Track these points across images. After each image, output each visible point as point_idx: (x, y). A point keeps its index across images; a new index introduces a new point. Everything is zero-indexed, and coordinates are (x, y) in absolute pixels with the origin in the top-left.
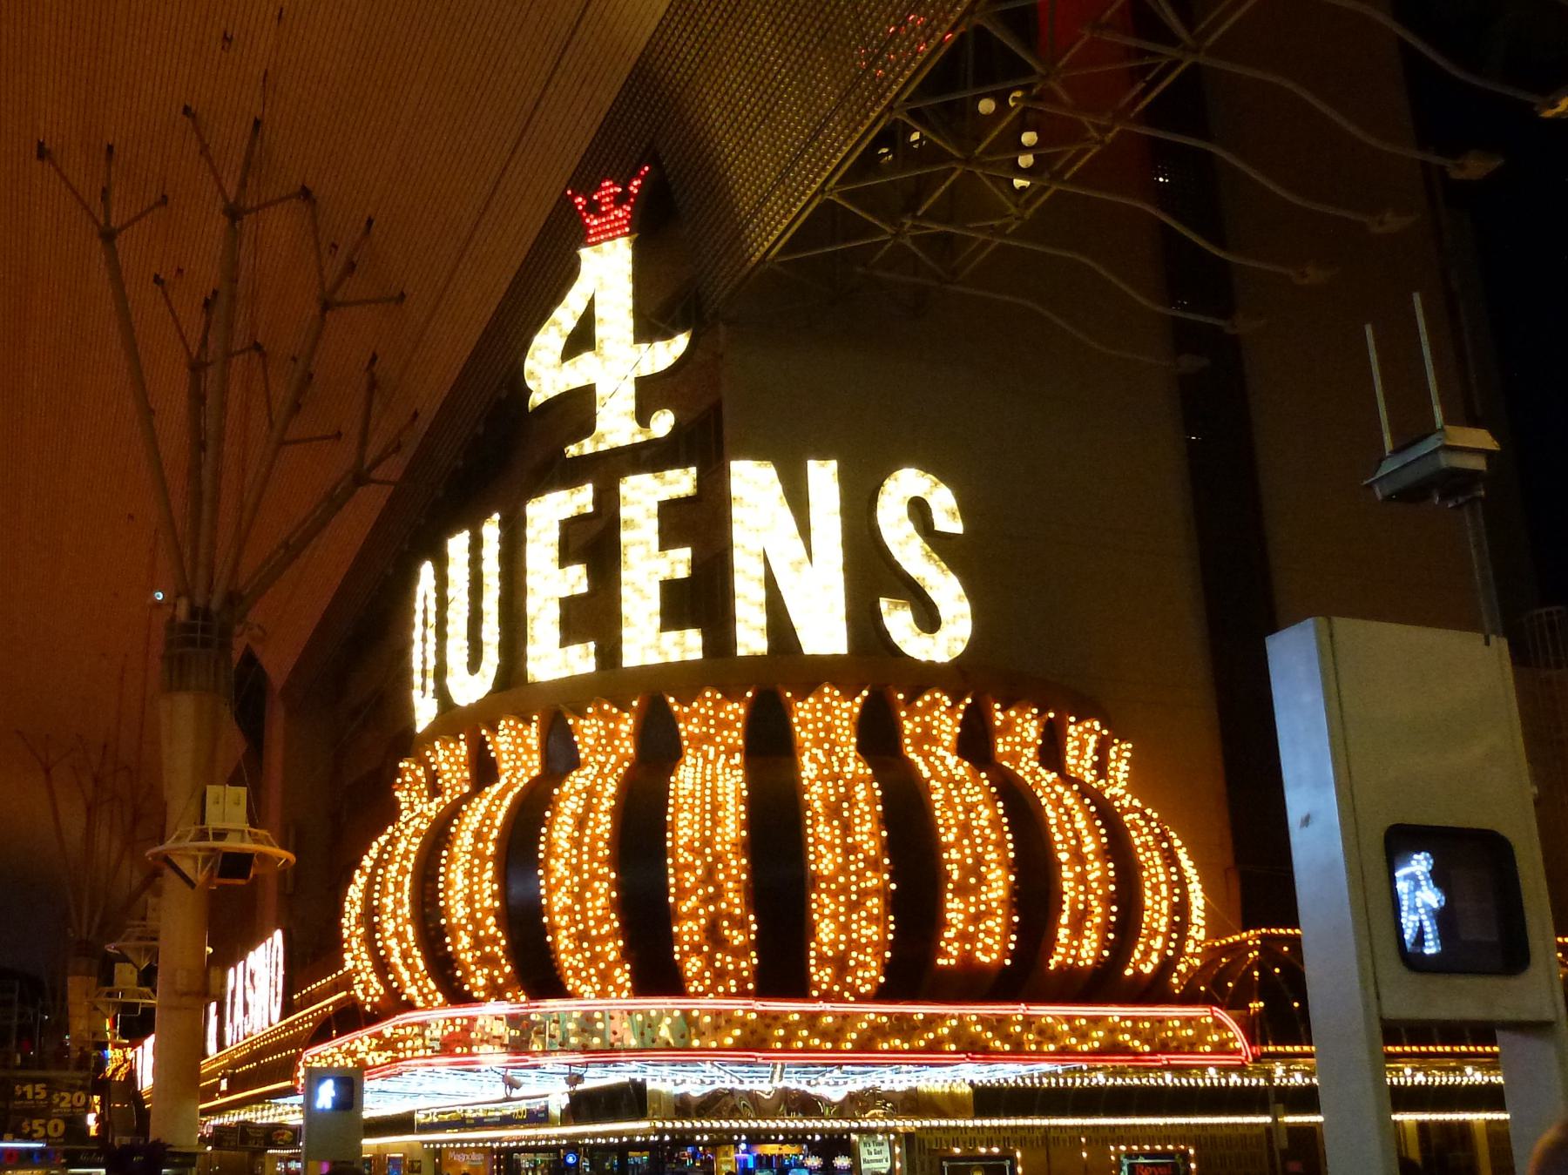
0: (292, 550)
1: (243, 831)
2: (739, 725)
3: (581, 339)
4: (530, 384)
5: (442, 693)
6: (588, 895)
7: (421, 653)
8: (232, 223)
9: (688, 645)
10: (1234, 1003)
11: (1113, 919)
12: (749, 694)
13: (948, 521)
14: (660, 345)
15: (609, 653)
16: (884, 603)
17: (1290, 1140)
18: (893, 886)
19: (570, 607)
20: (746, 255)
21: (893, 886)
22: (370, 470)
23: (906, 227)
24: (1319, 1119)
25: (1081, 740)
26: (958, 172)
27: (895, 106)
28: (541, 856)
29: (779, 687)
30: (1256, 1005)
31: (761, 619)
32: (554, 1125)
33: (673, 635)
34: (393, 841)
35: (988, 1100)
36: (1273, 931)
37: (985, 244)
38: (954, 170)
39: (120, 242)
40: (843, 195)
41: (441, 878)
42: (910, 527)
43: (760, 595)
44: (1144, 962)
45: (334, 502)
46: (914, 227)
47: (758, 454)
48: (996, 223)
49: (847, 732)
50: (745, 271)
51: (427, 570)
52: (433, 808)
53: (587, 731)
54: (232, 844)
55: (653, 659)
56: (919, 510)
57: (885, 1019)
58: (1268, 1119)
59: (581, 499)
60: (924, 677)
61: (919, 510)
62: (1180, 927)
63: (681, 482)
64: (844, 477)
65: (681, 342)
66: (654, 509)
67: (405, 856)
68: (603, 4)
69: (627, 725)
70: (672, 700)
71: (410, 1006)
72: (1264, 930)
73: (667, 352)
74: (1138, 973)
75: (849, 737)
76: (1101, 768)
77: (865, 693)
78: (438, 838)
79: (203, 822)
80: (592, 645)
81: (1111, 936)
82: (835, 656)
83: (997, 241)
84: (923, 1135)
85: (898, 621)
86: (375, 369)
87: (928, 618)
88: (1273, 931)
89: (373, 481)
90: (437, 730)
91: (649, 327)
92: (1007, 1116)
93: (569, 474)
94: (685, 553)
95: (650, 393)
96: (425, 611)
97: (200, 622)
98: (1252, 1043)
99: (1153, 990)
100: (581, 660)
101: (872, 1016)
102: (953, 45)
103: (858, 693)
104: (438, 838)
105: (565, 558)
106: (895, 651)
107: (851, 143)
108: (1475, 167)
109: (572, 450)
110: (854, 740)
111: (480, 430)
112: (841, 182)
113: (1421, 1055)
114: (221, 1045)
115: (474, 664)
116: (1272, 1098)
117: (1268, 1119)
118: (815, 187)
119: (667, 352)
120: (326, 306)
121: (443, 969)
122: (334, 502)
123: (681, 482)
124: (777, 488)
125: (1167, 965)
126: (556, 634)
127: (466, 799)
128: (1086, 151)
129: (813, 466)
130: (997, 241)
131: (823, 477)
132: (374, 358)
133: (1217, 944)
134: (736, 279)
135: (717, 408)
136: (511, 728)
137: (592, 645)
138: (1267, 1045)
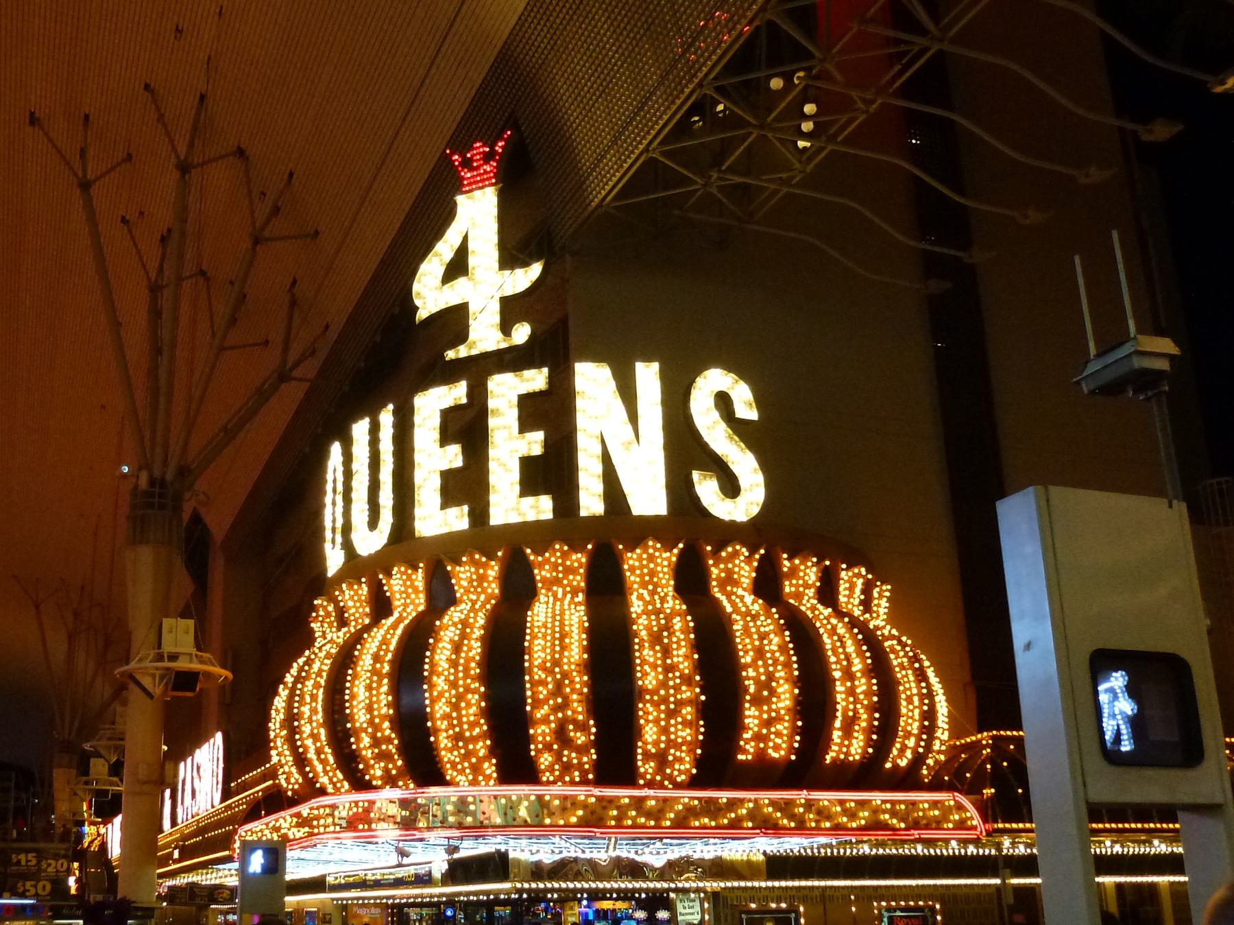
0: (230, 433)
1: (191, 655)
2: (582, 571)
3: (458, 267)
4: (417, 302)
5: (348, 546)
6: (463, 704)
7: (331, 514)
8: (183, 176)
9: (542, 508)
10: (971, 790)
11: (876, 723)
12: (590, 547)
13: (746, 410)
14: (519, 272)
15: (479, 514)
16: (696, 475)
17: (1015, 898)
18: (703, 698)
19: (448, 478)
20: (587, 201)
21: (703, 698)
22: (291, 370)
23: (713, 178)
24: (1038, 881)
25: (851, 583)
26: (754, 136)
27: (704, 83)
28: (426, 674)
29: (613, 541)
30: (989, 792)
31: (599, 487)
32: (436, 885)
33: (530, 500)
34: (309, 662)
35: (777, 866)
36: (1002, 733)
37: (775, 192)
38: (751, 133)
39: (94, 191)
40: (663, 154)
41: (347, 692)
42: (716, 415)
43: (598, 468)
44: (900, 757)
45: (262, 396)
46: (719, 179)
47: (596, 358)
48: (784, 175)
49: (667, 577)
50: (586, 214)
51: (336, 449)
52: (341, 636)
53: (462, 575)
54: (182, 664)
55: (514, 519)
56: (723, 401)
57: (696, 802)
58: (998, 881)
59: (457, 393)
60: (727, 533)
61: (723, 401)
62: (929, 729)
63: (536, 379)
64: (664, 376)
65: (536, 269)
66: (515, 401)
67: (319, 674)
68: (475, 3)
69: (493, 571)
70: (528, 551)
71: (323, 792)
72: (995, 732)
73: (525, 277)
74: (896, 766)
75: (668, 580)
76: (867, 604)
77: (681, 546)
78: (345, 660)
79: (159, 647)
80: (466, 508)
81: (874, 737)
82: (657, 517)
83: (785, 190)
84: (726, 893)
85: (707, 489)
86: (295, 290)
87: (731, 487)
88: (1002, 733)
89: (294, 379)
90: (344, 575)
91: (510, 258)
92: (793, 879)
93: (448, 373)
94: (539, 436)
95: (511, 309)
96: (335, 481)
97: (157, 490)
98: (985, 821)
99: (907, 780)
100: (457, 519)
101: (686, 800)
102: (750, 35)
103: (675, 546)
104: (345, 660)
105: (445, 439)
106: (704, 512)
107: (670, 113)
108: (1161, 131)
109: (450, 355)
110: (672, 583)
111: (378, 338)
112: (662, 143)
113: (1118, 831)
114: (174, 823)
115: (373, 523)
116: (1001, 864)
117: (998, 881)
118: (641, 147)
119: (525, 277)
120: (257, 241)
121: (349, 763)
122: (262, 396)
123: (536, 379)
124: (612, 385)
125: (918, 760)
126: (437, 499)
127: (367, 629)
128: (854, 119)
129: (640, 367)
130: (785, 190)
131: (648, 376)
132: (294, 282)
133: (958, 743)
134: (579, 219)
135: (564, 321)
136: (402, 573)
137: (466, 508)
138: (997, 822)
